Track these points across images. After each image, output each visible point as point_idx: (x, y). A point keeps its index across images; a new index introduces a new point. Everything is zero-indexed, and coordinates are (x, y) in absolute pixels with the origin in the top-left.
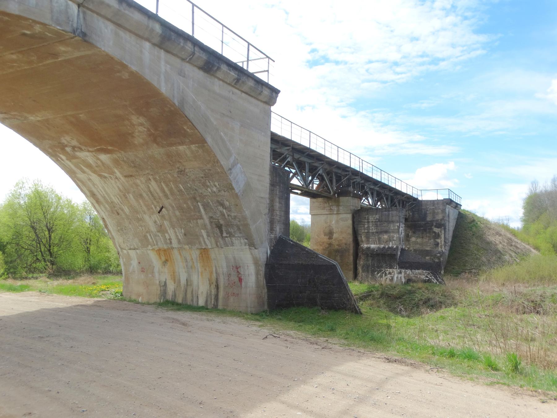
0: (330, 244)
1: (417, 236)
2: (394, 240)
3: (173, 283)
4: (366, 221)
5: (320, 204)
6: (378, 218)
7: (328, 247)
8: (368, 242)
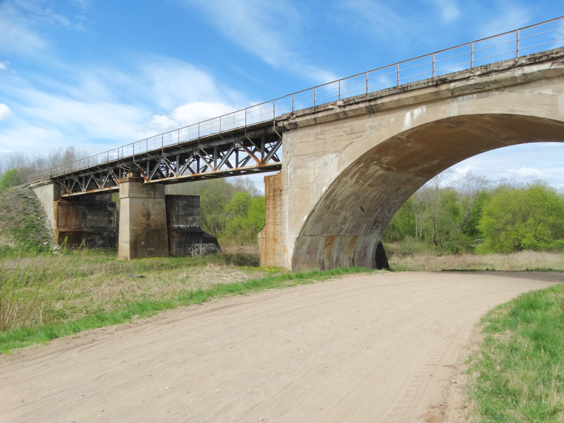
0: (148, 225)
1: (92, 214)
2: (196, 221)
3: (328, 261)
4: (176, 205)
5: (139, 188)
6: (185, 203)
7: (146, 228)
8: (178, 223)
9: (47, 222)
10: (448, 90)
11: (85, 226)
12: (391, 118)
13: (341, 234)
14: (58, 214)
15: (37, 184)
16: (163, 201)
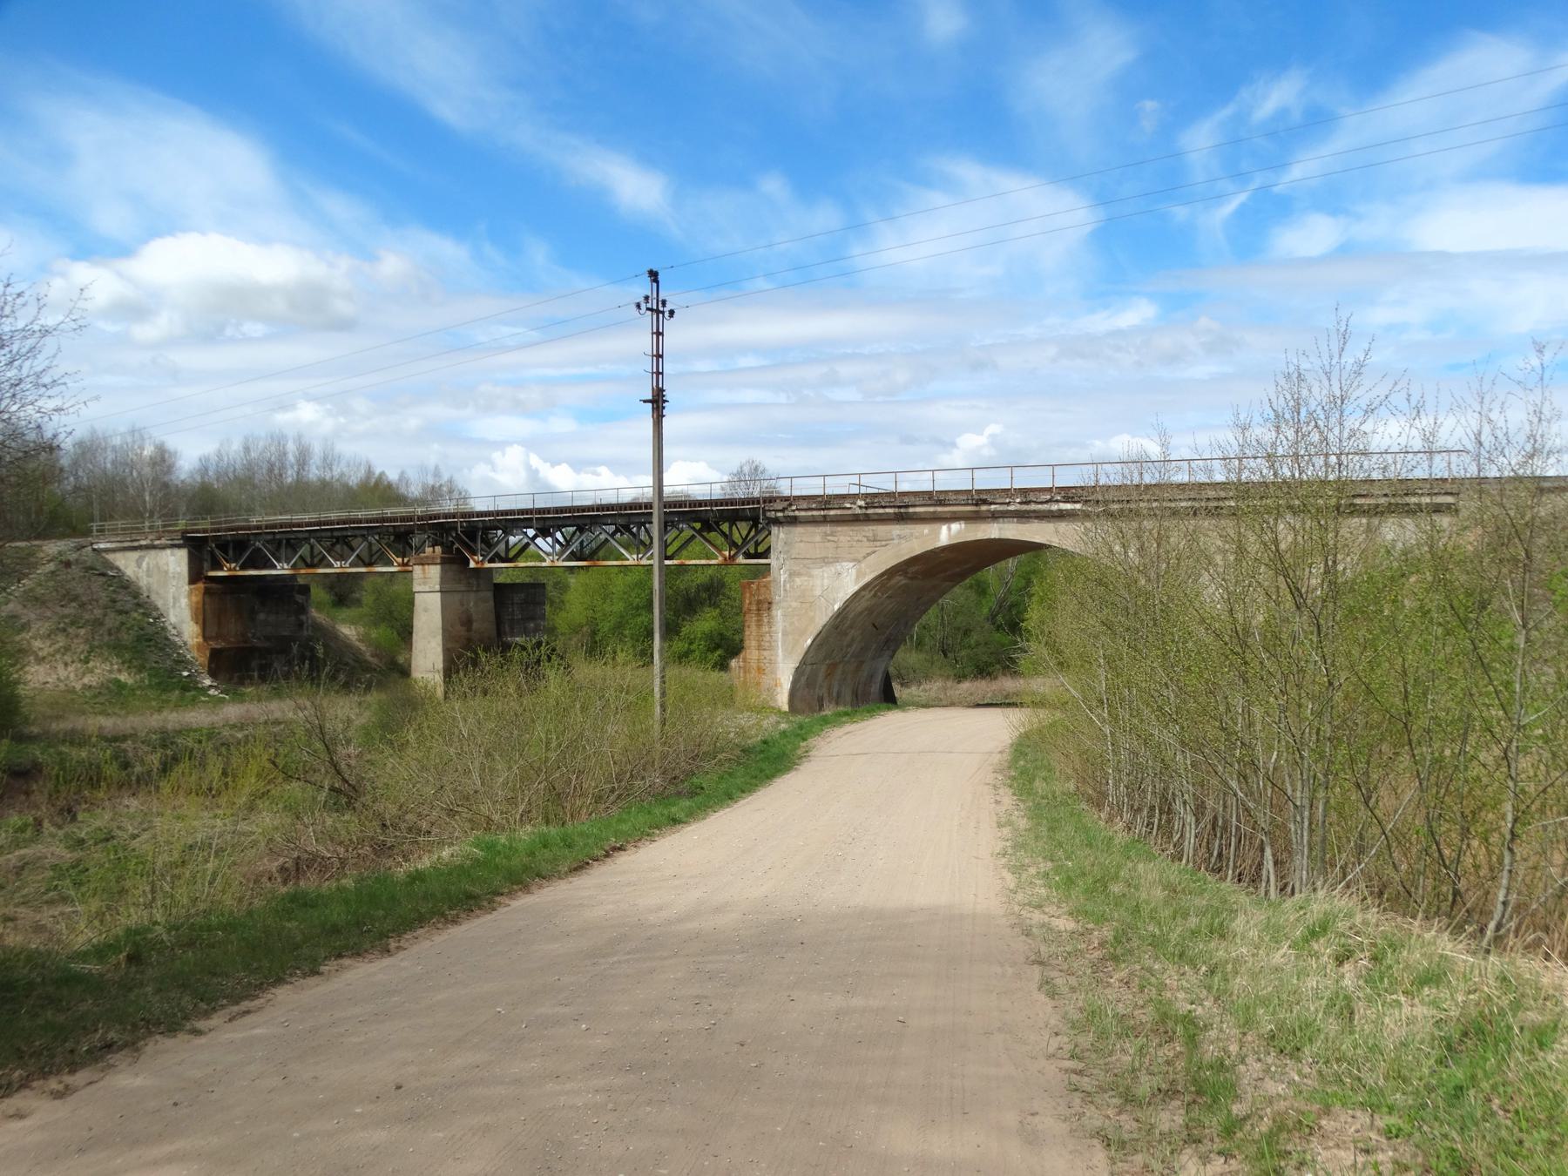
9: (170, 628)
10: (989, 511)
11: (254, 635)
12: (925, 529)
13: (846, 659)
14: (204, 610)
15: (119, 545)
16: (490, 595)
